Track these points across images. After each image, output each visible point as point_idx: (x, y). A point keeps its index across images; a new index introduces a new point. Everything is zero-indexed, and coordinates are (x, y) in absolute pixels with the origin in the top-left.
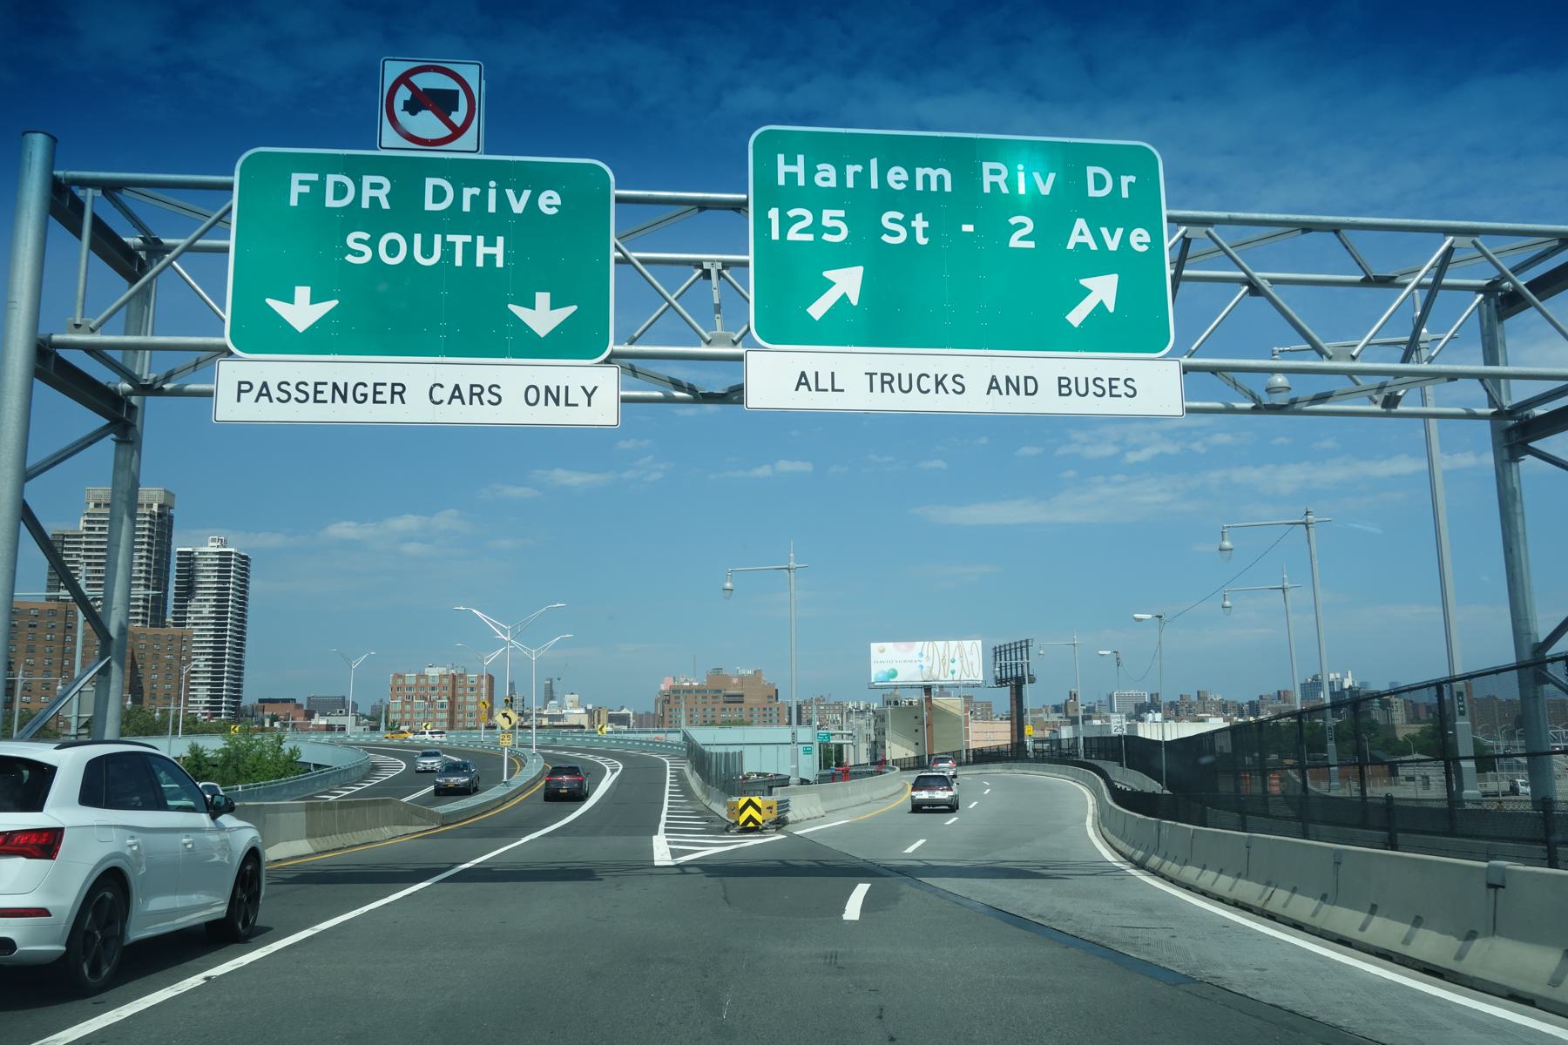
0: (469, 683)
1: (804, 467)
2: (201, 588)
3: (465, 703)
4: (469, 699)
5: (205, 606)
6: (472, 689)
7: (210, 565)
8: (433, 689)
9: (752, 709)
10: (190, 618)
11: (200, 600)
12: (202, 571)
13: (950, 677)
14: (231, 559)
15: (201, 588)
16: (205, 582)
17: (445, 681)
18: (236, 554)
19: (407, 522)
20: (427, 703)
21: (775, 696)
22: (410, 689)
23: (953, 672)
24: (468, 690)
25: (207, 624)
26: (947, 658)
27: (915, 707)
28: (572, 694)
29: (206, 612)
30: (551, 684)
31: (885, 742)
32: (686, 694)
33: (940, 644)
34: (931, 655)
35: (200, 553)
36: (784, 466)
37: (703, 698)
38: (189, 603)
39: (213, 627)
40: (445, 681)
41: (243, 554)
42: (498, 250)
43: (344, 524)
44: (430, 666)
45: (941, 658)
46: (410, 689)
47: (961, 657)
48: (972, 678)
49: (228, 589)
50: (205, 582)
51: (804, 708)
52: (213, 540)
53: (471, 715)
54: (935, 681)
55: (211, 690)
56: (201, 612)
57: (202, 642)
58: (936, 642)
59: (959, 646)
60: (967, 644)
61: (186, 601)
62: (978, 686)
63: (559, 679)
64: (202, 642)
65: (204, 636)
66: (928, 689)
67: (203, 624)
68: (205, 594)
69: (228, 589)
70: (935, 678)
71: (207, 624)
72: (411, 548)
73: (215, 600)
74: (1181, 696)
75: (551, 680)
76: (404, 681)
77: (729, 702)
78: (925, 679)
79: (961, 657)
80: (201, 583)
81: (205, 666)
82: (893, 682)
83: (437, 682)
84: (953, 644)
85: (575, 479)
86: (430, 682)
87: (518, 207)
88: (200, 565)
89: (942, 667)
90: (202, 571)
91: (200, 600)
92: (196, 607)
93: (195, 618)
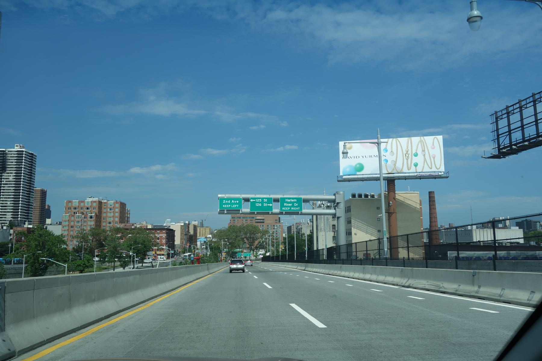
0: (109, 206)
1: (295, 147)
2: (9, 168)
3: (107, 216)
4: (109, 215)
5: (10, 176)
6: (111, 209)
7: (13, 157)
8: (88, 209)
9: (268, 226)
10: (3, 181)
11: (8, 173)
12: (10, 159)
13: (413, 169)
14: (23, 154)
15: (9, 168)
16: (11, 165)
17: (94, 204)
18: (26, 152)
19: (157, 168)
20: (83, 216)
21: (278, 220)
22: (75, 208)
23: (416, 165)
24: (109, 210)
25: (11, 184)
26: (410, 152)
27: (377, 199)
28: (195, 221)
29: (11, 178)
30: (202, 222)
31: (351, 229)
32: (238, 219)
33: (403, 141)
34: (394, 150)
35: (9, 151)
36: (288, 147)
37: (246, 220)
38: (3, 174)
39: (14, 185)
40: (94, 204)
41: (30, 152)
42: (286, 200)
43: (136, 168)
44: (90, 197)
45: (405, 152)
46: (75, 208)
47: (424, 151)
48: (434, 169)
49: (22, 168)
50: (11, 165)
51: (292, 227)
52: (17, 146)
53: (110, 223)
54: (398, 173)
55: (12, 215)
56: (8, 179)
57: (9, 192)
58: (399, 139)
59: (421, 141)
60: (429, 139)
61: (2, 173)
62: (440, 177)
63: (205, 220)
64: (9, 192)
65: (10, 190)
66: (391, 182)
67: (10, 184)
68: (10, 170)
69: (22, 168)
70: (399, 171)
71: (11, 184)
72: (159, 177)
73: (15, 173)
74: (441, 226)
75: (202, 220)
76: (72, 204)
77: (258, 223)
78: (390, 172)
79: (424, 151)
80: (9, 165)
81: (10, 203)
82: (360, 175)
83: (90, 204)
84: (416, 140)
85: (215, 152)
86: (86, 205)
87: (235, 202)
88: (9, 157)
89: (405, 161)
90: (10, 159)
91: (8, 173)
92: (6, 176)
93: (6, 181)
